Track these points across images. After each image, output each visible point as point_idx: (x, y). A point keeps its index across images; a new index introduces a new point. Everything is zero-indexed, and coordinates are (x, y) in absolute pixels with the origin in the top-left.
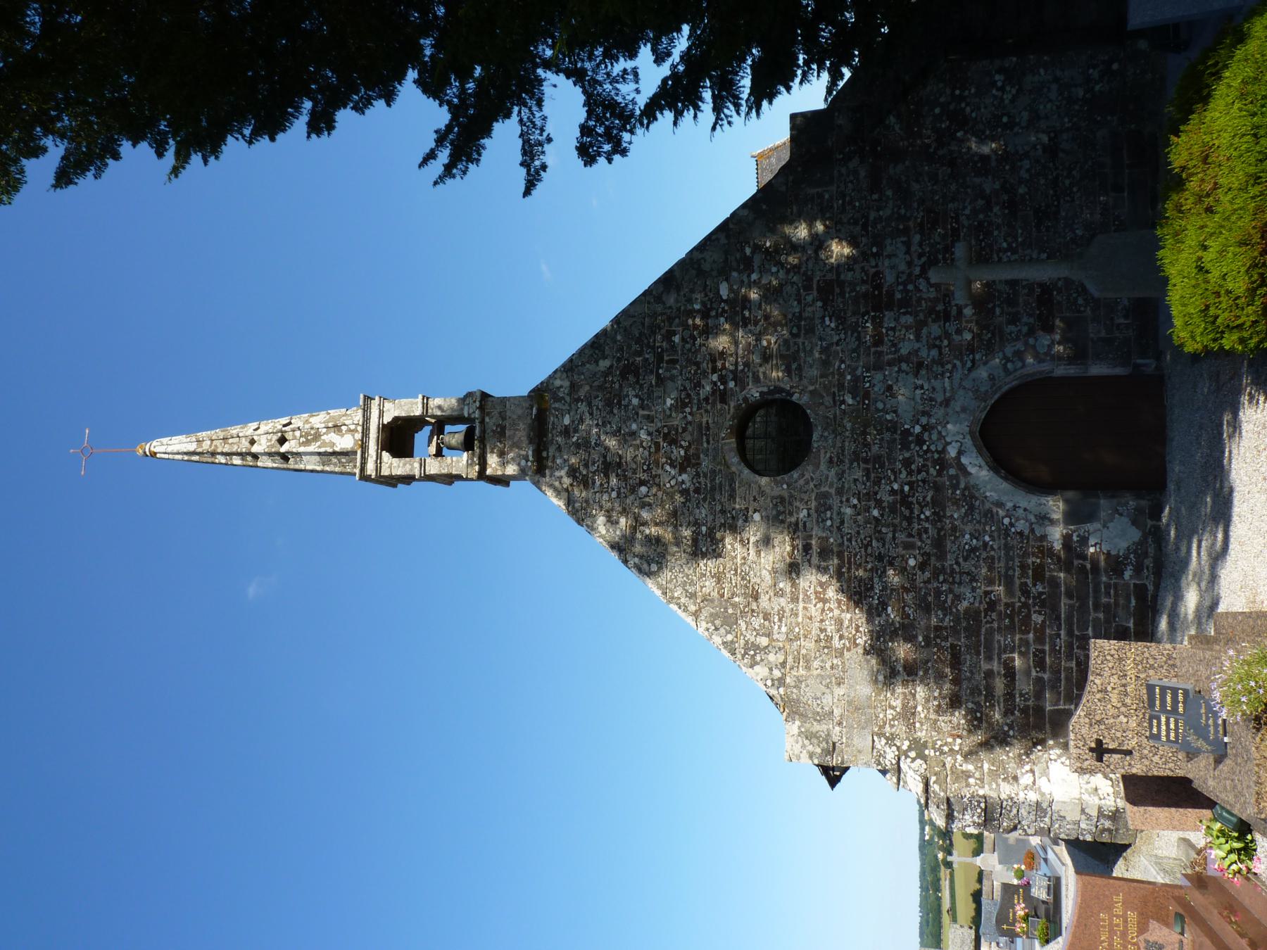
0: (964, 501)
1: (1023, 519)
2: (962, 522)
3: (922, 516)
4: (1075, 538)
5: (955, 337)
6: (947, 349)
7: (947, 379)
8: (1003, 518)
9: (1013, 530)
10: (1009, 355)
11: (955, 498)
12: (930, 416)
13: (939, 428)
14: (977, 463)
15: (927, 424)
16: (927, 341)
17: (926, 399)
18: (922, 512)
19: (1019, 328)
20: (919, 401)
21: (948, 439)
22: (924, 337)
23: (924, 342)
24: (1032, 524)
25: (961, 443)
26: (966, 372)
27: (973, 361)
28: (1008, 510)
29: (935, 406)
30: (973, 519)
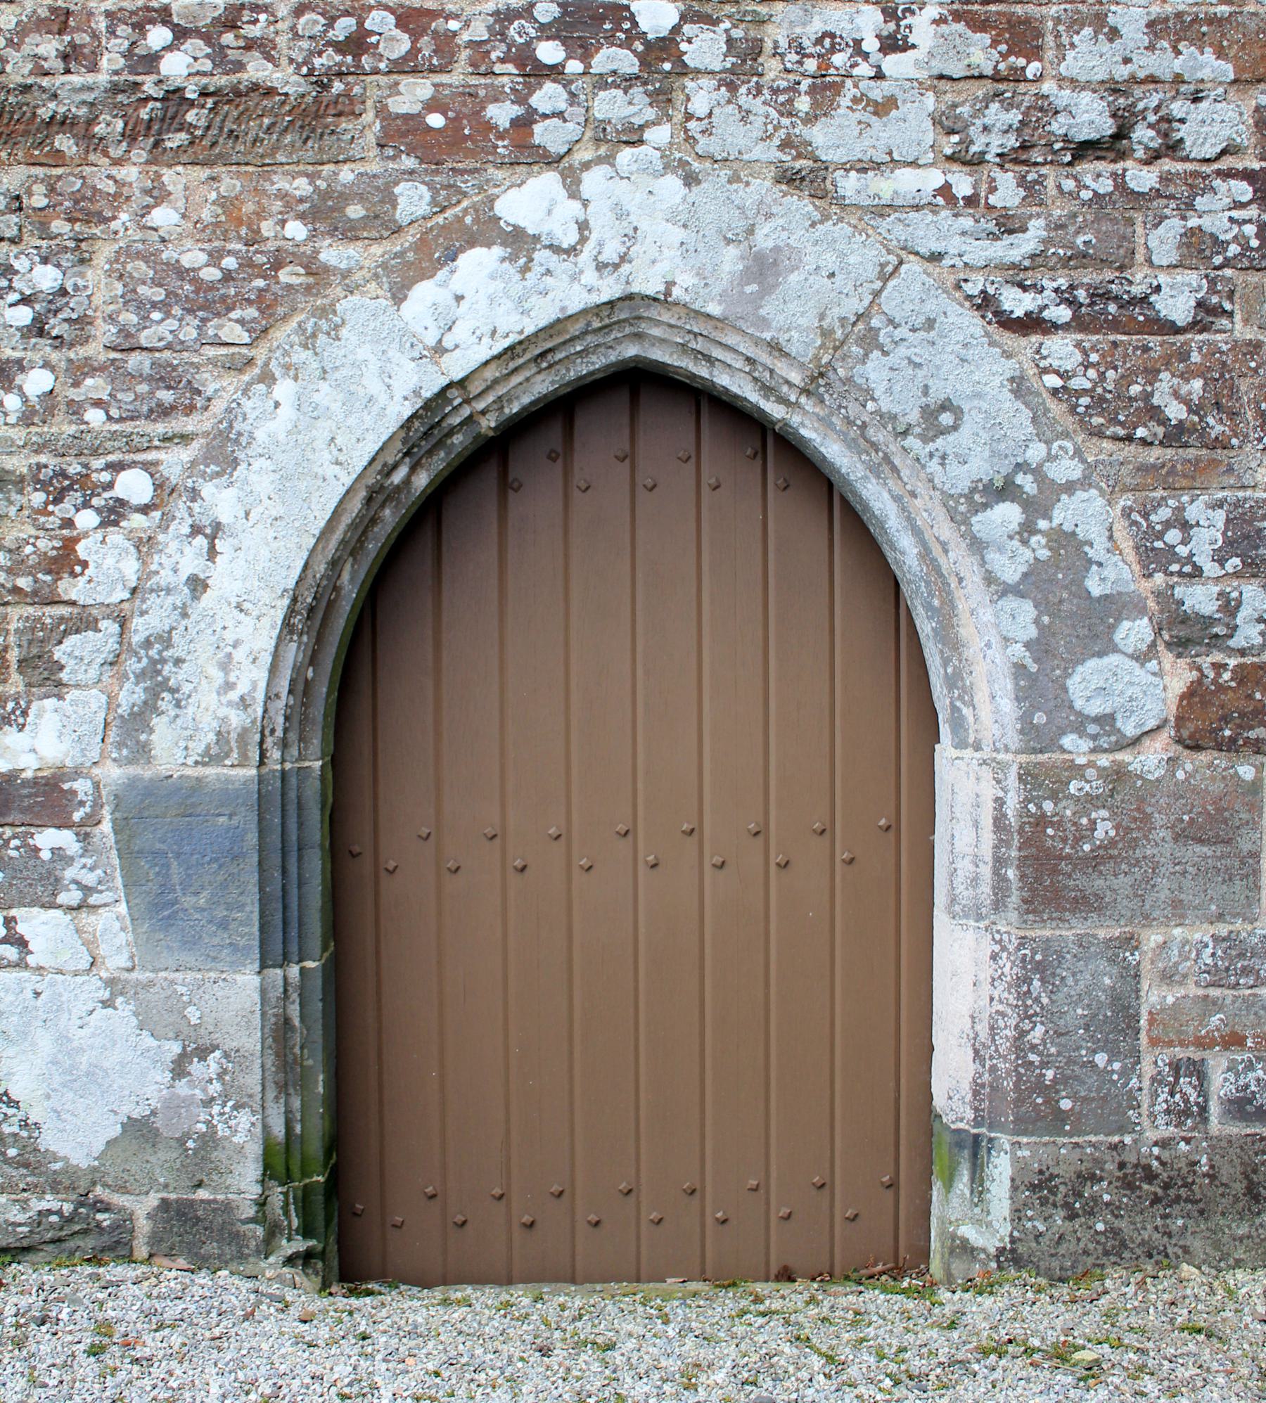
0: (247, 263)
1: (146, 574)
2: (128, 253)
3: (158, 36)
4: (48, 839)
5: (1173, 228)
6: (1106, 186)
7: (936, 178)
8: (147, 466)
9: (86, 520)
10: (1065, 514)
11: (261, 214)
12: (729, 82)
13: (659, 135)
14: (461, 334)
15: (683, 70)
16: (1152, 80)
17: (824, 61)
18: (181, 34)
19: (1211, 569)
20: (817, 26)
21: (593, 182)
22: (1178, 65)
23: (1147, 63)
24: (123, 622)
25: (572, 251)
26: (973, 289)
27: (1032, 324)
28: (194, 494)
29: (787, 110)
30: (143, 308)
